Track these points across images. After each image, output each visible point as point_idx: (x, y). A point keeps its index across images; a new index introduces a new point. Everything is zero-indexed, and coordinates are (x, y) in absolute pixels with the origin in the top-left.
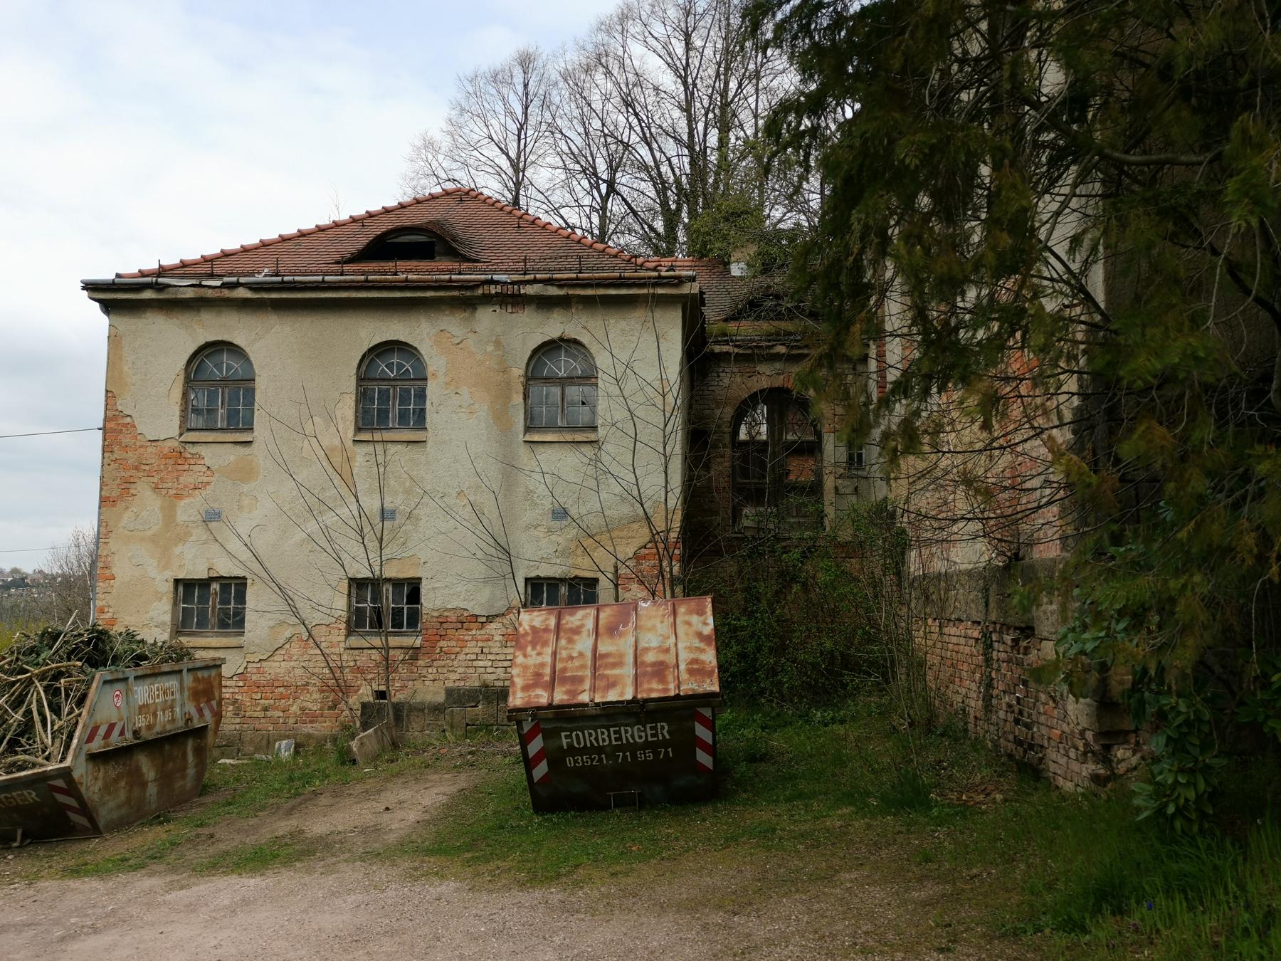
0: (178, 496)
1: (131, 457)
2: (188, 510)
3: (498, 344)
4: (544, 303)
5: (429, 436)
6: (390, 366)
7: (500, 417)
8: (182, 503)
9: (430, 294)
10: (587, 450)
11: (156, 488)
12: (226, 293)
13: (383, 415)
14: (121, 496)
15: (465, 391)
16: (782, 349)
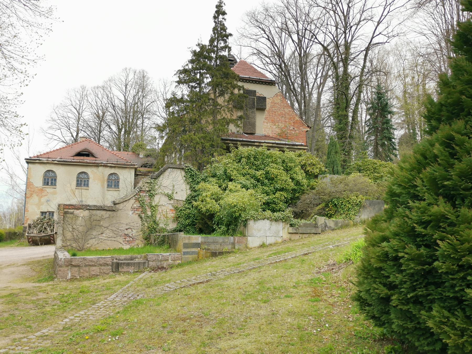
0: (41, 197)
1: (32, 190)
2: (43, 200)
3: (103, 173)
4: (111, 167)
6: (82, 176)
7: (103, 186)
8: (42, 198)
9: (91, 164)
10: (117, 191)
11: (37, 195)
12: (53, 162)
13: (81, 184)
14: (30, 197)
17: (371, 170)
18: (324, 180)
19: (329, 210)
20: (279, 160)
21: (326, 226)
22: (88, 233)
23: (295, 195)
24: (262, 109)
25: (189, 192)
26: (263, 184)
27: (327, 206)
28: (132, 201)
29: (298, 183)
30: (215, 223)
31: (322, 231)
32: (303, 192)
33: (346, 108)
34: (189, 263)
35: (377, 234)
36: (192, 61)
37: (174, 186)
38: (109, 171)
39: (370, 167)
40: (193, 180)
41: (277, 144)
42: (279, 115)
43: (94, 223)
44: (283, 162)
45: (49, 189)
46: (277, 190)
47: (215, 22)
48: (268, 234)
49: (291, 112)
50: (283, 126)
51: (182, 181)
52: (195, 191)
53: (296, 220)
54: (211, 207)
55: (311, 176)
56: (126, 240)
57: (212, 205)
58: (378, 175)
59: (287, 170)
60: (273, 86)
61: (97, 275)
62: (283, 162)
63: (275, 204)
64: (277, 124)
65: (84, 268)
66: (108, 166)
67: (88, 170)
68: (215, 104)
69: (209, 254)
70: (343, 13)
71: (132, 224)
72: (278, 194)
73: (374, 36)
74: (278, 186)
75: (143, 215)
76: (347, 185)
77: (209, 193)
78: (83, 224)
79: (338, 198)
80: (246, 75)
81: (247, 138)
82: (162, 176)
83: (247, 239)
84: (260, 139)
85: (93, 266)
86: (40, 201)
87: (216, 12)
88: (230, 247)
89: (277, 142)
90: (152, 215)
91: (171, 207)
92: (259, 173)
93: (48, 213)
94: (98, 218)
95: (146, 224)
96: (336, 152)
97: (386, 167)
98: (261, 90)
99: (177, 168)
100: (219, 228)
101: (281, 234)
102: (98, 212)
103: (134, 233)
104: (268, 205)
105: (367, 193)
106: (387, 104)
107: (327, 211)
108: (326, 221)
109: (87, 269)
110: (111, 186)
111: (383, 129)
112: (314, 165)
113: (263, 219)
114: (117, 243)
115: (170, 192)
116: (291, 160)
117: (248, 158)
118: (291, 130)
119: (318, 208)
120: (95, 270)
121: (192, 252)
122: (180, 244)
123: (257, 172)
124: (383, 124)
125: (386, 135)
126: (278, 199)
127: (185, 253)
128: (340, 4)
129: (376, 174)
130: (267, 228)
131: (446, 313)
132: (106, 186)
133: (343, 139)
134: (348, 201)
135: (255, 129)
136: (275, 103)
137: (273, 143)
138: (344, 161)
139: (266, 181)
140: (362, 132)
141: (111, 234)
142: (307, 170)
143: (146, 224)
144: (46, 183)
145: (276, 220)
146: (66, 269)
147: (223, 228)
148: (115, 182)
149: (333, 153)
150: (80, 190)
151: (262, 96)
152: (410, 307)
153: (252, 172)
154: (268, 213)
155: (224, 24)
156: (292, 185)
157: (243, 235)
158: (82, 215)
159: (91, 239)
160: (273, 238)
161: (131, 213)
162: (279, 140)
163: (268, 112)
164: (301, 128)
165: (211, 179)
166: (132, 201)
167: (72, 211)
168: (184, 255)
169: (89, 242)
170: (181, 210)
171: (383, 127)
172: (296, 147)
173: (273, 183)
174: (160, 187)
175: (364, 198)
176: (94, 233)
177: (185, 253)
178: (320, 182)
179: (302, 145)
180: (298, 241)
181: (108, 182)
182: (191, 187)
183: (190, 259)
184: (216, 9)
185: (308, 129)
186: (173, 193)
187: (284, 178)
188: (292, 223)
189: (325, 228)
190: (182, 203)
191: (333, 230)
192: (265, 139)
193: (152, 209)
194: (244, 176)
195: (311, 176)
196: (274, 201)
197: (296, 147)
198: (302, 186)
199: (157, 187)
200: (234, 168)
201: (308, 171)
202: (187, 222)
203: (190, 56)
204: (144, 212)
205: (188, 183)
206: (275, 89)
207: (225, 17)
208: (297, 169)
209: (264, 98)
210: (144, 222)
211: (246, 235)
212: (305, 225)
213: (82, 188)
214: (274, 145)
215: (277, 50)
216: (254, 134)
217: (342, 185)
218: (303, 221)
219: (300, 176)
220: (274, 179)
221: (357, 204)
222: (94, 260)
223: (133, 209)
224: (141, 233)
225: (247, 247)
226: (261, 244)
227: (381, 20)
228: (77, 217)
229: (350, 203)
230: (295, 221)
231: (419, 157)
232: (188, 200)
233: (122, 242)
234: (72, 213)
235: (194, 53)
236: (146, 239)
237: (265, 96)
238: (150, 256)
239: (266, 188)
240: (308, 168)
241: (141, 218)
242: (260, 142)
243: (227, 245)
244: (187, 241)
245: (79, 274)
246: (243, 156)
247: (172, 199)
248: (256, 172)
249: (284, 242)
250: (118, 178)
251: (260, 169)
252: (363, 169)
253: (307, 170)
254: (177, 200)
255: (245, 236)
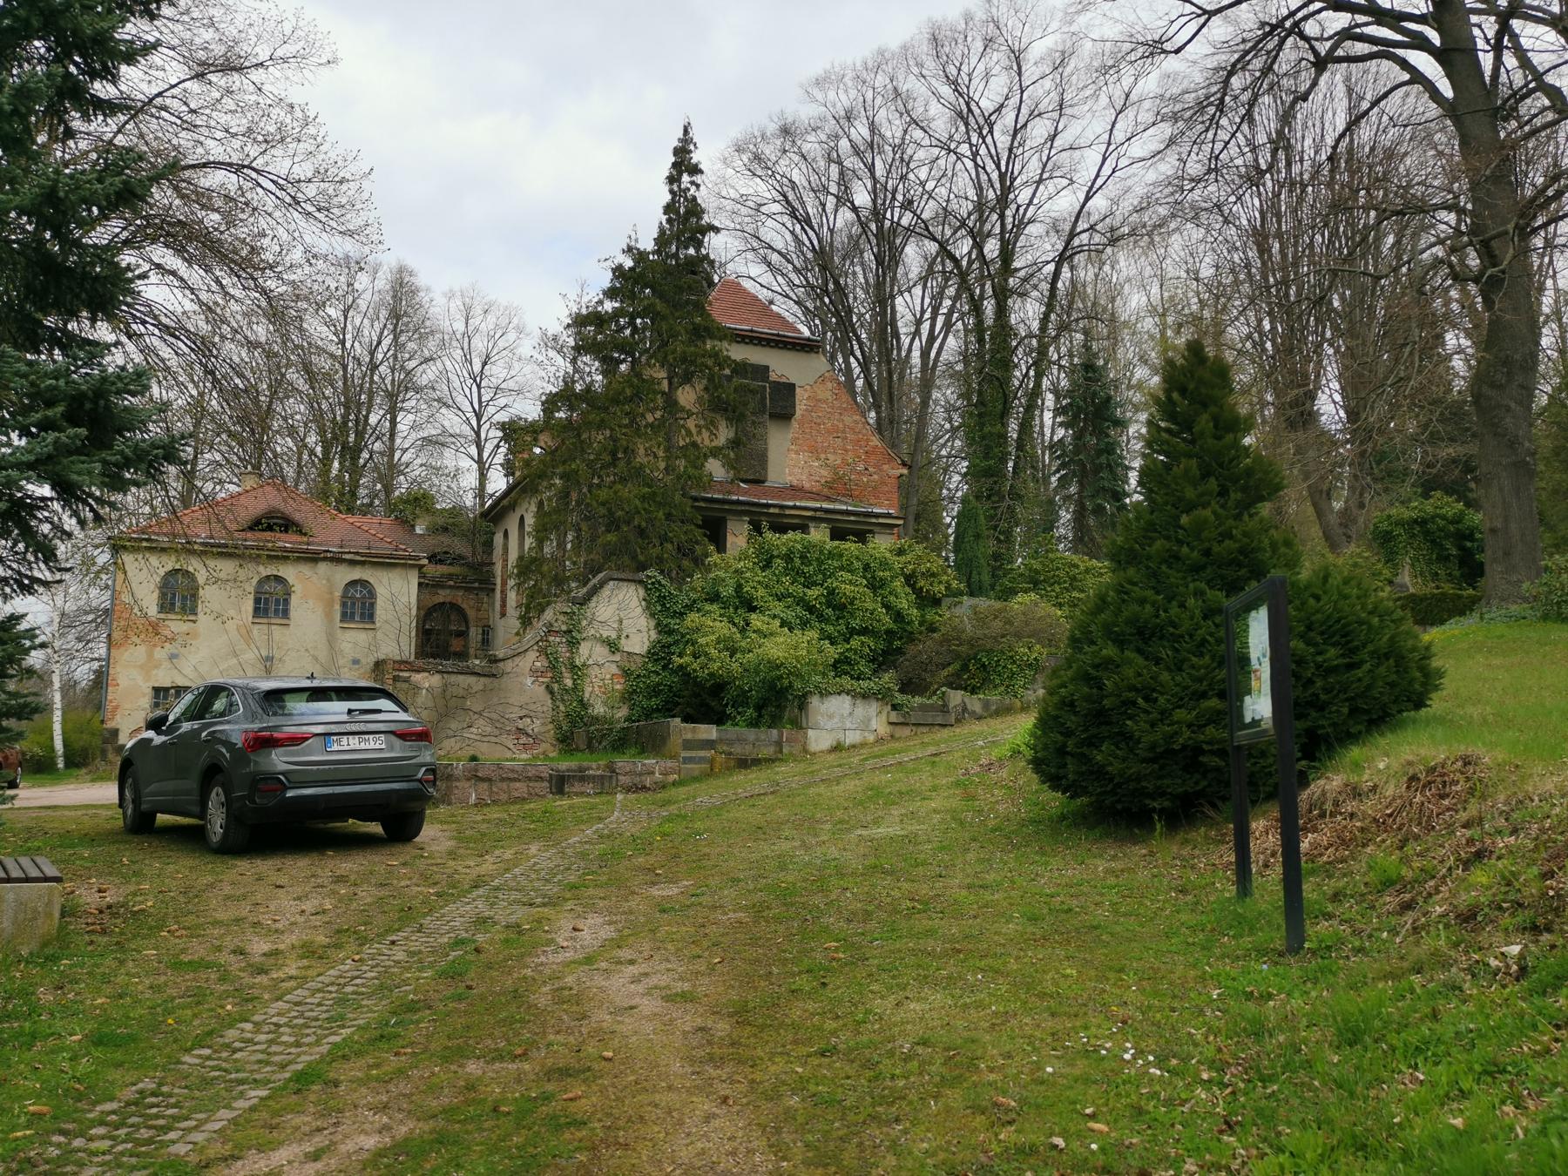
3: (328, 580)
4: (352, 563)
5: (292, 623)
7: (328, 615)
10: (370, 632)
13: (266, 611)
15: (311, 602)
16: (451, 583)
17: (1065, 582)
18: (958, 611)
19: (969, 679)
20: (857, 564)
21: (965, 709)
22: (441, 724)
23: (892, 644)
24: (784, 414)
25: (654, 635)
26: (821, 618)
27: (965, 668)
28: (532, 655)
29: (899, 616)
30: (727, 705)
31: (958, 721)
32: (911, 638)
33: (1002, 417)
34: (696, 779)
35: (1055, 682)
36: (611, 293)
37: (621, 622)
38: (170, 563)
39: (1061, 574)
40: (665, 609)
41: (827, 511)
42: (828, 432)
43: (453, 703)
44: (867, 567)
45: (175, 625)
46: (853, 632)
47: (671, 191)
48: (848, 725)
49: (860, 426)
50: (839, 462)
51: (639, 610)
52: (670, 632)
53: (905, 697)
54: (720, 668)
55: (928, 601)
56: (521, 742)
57: (719, 663)
58: (1082, 596)
59: (876, 585)
60: (813, 355)
61: (524, 799)
62: (867, 567)
63: (850, 664)
64: (823, 456)
65: (499, 784)
66: (345, 561)
67: (289, 572)
68: (671, 404)
69: (732, 763)
70: (998, 166)
71: (533, 707)
72: (855, 642)
73: (1078, 230)
74: (855, 624)
75: (556, 687)
76: (1009, 622)
77: (713, 638)
78: (430, 704)
79: (989, 652)
80: (741, 321)
81: (746, 493)
82: (595, 599)
83: (806, 734)
84: (779, 497)
85: (515, 780)
86: (150, 655)
87: (675, 165)
88: (772, 749)
89: (825, 505)
90: (575, 688)
91: (614, 669)
92: (813, 593)
93: (173, 691)
94: (461, 692)
95: (562, 708)
96: (978, 536)
97: (1102, 574)
98: (782, 366)
99: (629, 580)
100: (739, 713)
101: (874, 724)
102: (461, 677)
103: (536, 726)
104: (841, 666)
105: (1050, 640)
106: (1109, 398)
107: (966, 680)
108: (966, 700)
109: (504, 785)
110: (353, 614)
111: (1097, 469)
112: (933, 575)
113: (839, 694)
114: (501, 748)
115: (614, 635)
116: (884, 564)
117: (788, 558)
118: (860, 473)
119: (945, 673)
120: (520, 788)
121: (700, 758)
122: (675, 741)
123: (810, 592)
124: (1099, 453)
125: (1106, 484)
126: (855, 653)
127: (687, 760)
128: (989, 139)
129: (1075, 594)
130: (846, 713)
131: (1113, 747)
132: (338, 616)
133: (995, 498)
134: (1011, 657)
135: (765, 469)
136: (820, 400)
137: (816, 510)
138: (997, 557)
139: (829, 611)
140: (1044, 461)
141: (489, 729)
142: (918, 586)
143: (562, 708)
144: (166, 605)
145: (865, 696)
146: (467, 785)
147: (750, 712)
148: (364, 604)
149: (969, 538)
150: (265, 627)
151: (784, 380)
152: (1085, 750)
153: (798, 590)
154: (846, 681)
155: (694, 198)
156: (887, 621)
157: (797, 724)
158: (427, 685)
159: (447, 737)
160: (858, 732)
161: (529, 681)
162: (828, 499)
163: (801, 424)
164: (886, 467)
165: (708, 607)
166: (532, 655)
167: (406, 674)
168: (684, 763)
169: (443, 745)
170: (639, 676)
171: (1097, 462)
172: (874, 520)
173: (844, 617)
174: (590, 623)
175: (1045, 651)
176: (454, 725)
177: (687, 760)
178: (948, 615)
179: (888, 516)
180: (908, 738)
181: (344, 605)
182: (658, 625)
183: (696, 773)
184: (673, 159)
185: (905, 471)
186: (619, 637)
187: (869, 605)
188: (896, 701)
189: (963, 714)
190: (639, 660)
191: (980, 718)
192: (793, 498)
193: (576, 674)
194: (780, 600)
195: (928, 601)
196: (846, 657)
197: (874, 520)
198: (908, 623)
199: (584, 623)
200: (759, 582)
201: (921, 588)
202: (654, 702)
203: (605, 280)
204: (557, 679)
205: (652, 615)
206: (819, 363)
207: (698, 179)
208: (898, 584)
209: (791, 388)
210: (558, 703)
211: (804, 725)
212: (922, 707)
213: (273, 621)
214: (819, 514)
215: (816, 242)
216: (763, 482)
217: (998, 624)
218: (918, 699)
219: (905, 601)
220: (845, 607)
221: (1031, 664)
222: (516, 768)
223: (534, 672)
224: (551, 726)
225: (806, 751)
226: (835, 743)
227: (1097, 186)
228: (417, 688)
229: (1014, 662)
230: (900, 698)
231: (1099, 602)
232: (653, 654)
233: (512, 747)
234: (407, 680)
235: (618, 271)
236: (562, 742)
237: (792, 380)
238: (620, 764)
239: (830, 629)
240: (921, 583)
241: (552, 693)
242: (782, 507)
243: (766, 746)
244: (689, 736)
245: (490, 796)
246: (775, 553)
247: (618, 650)
248: (806, 590)
249: (880, 740)
250: (372, 594)
251: (815, 584)
252: (1044, 581)
253: (918, 586)
254: (629, 653)
255: (801, 728)
